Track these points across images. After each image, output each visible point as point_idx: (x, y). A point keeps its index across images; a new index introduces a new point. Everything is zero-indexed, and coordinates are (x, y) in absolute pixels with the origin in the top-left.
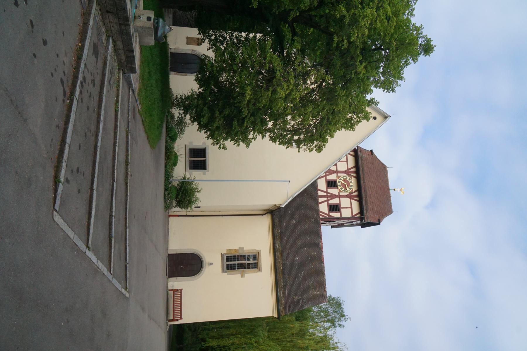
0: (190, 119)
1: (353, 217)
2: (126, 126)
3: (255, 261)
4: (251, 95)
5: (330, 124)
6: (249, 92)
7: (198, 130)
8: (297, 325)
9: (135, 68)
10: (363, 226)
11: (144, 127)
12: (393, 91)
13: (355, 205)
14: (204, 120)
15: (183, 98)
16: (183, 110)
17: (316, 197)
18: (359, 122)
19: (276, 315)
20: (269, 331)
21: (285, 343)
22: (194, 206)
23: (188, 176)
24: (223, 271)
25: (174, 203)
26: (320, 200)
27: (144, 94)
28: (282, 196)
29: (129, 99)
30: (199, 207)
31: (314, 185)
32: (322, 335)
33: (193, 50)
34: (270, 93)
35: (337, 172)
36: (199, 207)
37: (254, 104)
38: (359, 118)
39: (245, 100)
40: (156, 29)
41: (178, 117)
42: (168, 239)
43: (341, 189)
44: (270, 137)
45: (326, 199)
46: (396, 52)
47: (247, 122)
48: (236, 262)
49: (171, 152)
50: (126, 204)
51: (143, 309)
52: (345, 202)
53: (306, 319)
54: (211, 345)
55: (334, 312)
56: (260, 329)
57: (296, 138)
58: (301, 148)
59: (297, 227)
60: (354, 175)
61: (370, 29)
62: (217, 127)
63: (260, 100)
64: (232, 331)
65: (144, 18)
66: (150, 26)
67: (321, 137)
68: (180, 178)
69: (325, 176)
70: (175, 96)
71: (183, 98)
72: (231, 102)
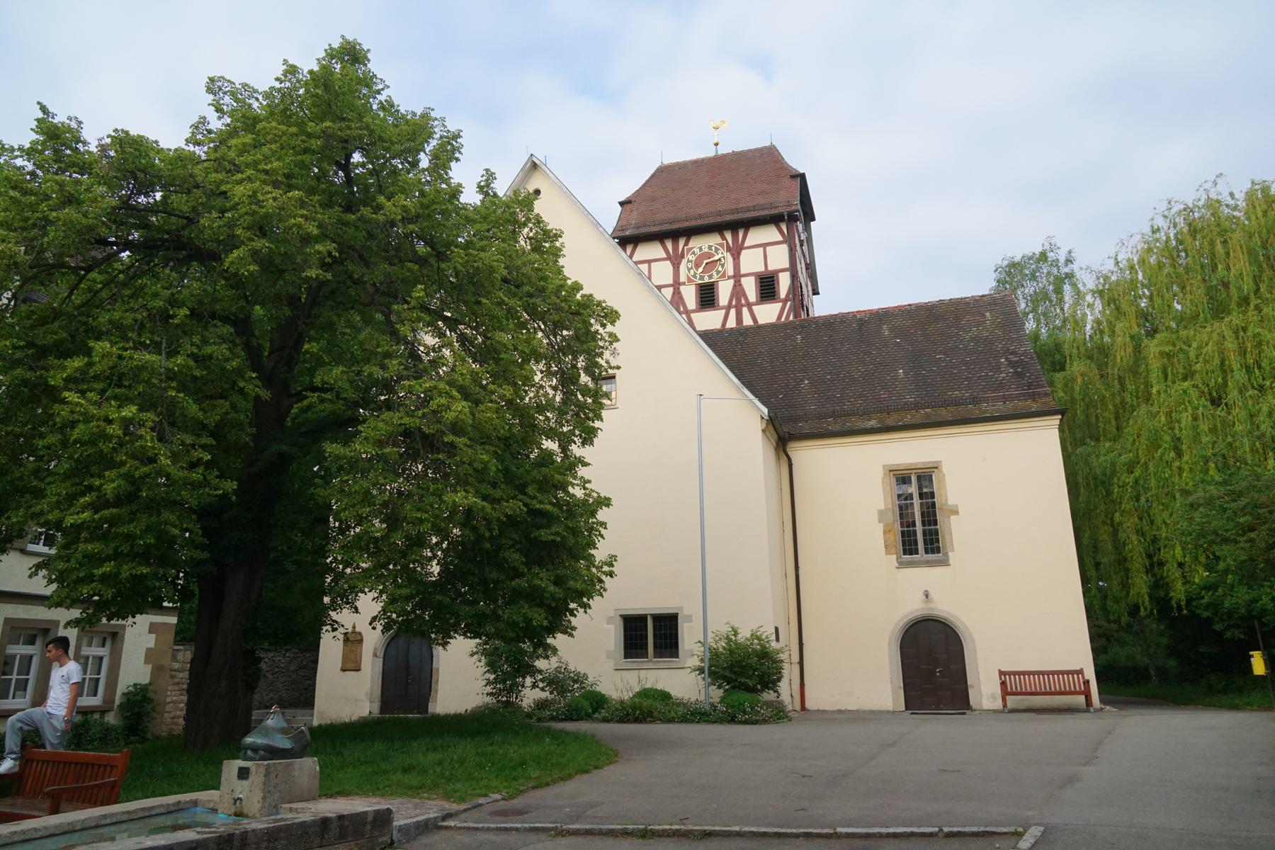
0: (547, 657)
1: (789, 240)
2: (543, 836)
3: (914, 478)
4: (466, 491)
5: (543, 290)
6: (461, 498)
7: (571, 635)
8: (1076, 367)
9: (377, 812)
10: (809, 216)
11: (555, 782)
12: (457, 136)
13: (757, 236)
14: (539, 617)
15: (492, 677)
16: (524, 677)
17: (741, 331)
18: (539, 221)
19: (1055, 421)
20: (1098, 440)
21: (1127, 395)
22: (774, 644)
23: (695, 662)
24: (945, 562)
25: (769, 696)
26: (747, 321)
27: (459, 786)
28: (739, 416)
29: (468, 828)
30: (777, 629)
31: (709, 338)
32: (1098, 302)
33: (375, 655)
34: (461, 441)
35: (676, 285)
36: (777, 629)
37: (494, 485)
38: (529, 220)
39: (483, 508)
40: (274, 752)
41: (542, 689)
42: (864, 712)
43: (718, 272)
44: (583, 444)
45: (745, 310)
46: (349, 120)
47: (541, 502)
48: (919, 528)
49: (634, 708)
50: (765, 835)
51: (1071, 780)
52: (752, 262)
53: (1058, 347)
54: (1145, 590)
55: (1033, 277)
56: (1094, 461)
57: (584, 379)
58: (607, 362)
59: (817, 378)
60: (682, 242)
61: (290, 187)
62: (556, 583)
63: (480, 466)
64: (1104, 534)
65: (243, 789)
66: (262, 770)
67: (577, 313)
68: (702, 683)
69: (687, 312)
70: (488, 699)
71: (492, 677)
72: (488, 546)
